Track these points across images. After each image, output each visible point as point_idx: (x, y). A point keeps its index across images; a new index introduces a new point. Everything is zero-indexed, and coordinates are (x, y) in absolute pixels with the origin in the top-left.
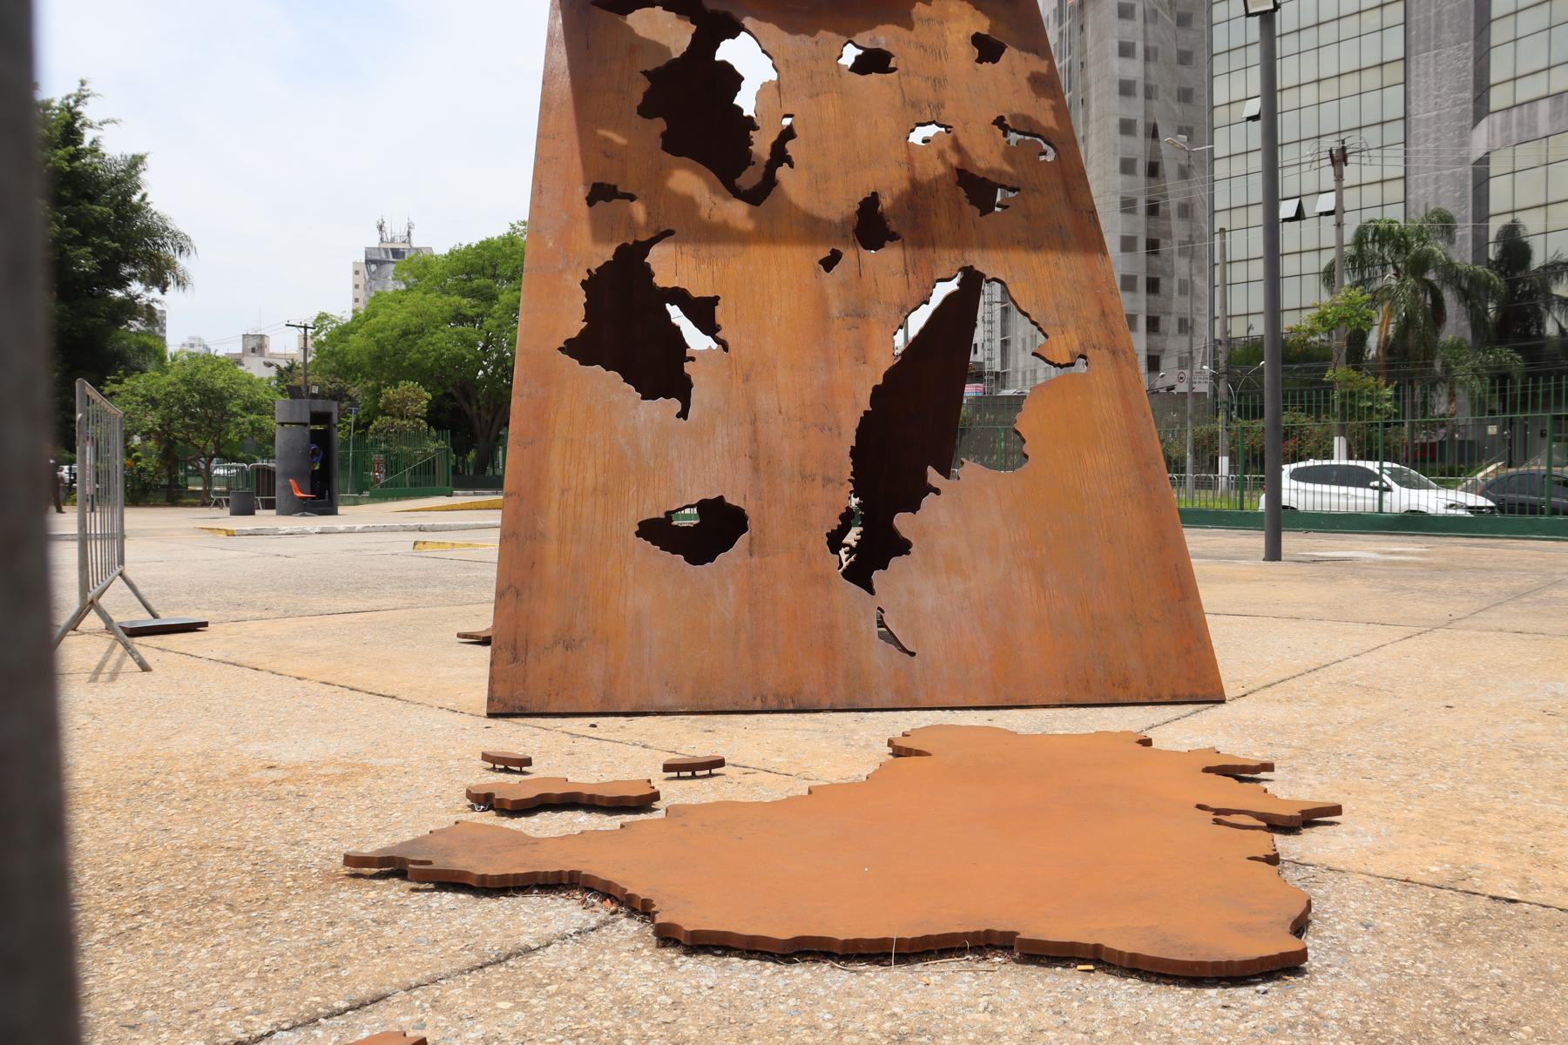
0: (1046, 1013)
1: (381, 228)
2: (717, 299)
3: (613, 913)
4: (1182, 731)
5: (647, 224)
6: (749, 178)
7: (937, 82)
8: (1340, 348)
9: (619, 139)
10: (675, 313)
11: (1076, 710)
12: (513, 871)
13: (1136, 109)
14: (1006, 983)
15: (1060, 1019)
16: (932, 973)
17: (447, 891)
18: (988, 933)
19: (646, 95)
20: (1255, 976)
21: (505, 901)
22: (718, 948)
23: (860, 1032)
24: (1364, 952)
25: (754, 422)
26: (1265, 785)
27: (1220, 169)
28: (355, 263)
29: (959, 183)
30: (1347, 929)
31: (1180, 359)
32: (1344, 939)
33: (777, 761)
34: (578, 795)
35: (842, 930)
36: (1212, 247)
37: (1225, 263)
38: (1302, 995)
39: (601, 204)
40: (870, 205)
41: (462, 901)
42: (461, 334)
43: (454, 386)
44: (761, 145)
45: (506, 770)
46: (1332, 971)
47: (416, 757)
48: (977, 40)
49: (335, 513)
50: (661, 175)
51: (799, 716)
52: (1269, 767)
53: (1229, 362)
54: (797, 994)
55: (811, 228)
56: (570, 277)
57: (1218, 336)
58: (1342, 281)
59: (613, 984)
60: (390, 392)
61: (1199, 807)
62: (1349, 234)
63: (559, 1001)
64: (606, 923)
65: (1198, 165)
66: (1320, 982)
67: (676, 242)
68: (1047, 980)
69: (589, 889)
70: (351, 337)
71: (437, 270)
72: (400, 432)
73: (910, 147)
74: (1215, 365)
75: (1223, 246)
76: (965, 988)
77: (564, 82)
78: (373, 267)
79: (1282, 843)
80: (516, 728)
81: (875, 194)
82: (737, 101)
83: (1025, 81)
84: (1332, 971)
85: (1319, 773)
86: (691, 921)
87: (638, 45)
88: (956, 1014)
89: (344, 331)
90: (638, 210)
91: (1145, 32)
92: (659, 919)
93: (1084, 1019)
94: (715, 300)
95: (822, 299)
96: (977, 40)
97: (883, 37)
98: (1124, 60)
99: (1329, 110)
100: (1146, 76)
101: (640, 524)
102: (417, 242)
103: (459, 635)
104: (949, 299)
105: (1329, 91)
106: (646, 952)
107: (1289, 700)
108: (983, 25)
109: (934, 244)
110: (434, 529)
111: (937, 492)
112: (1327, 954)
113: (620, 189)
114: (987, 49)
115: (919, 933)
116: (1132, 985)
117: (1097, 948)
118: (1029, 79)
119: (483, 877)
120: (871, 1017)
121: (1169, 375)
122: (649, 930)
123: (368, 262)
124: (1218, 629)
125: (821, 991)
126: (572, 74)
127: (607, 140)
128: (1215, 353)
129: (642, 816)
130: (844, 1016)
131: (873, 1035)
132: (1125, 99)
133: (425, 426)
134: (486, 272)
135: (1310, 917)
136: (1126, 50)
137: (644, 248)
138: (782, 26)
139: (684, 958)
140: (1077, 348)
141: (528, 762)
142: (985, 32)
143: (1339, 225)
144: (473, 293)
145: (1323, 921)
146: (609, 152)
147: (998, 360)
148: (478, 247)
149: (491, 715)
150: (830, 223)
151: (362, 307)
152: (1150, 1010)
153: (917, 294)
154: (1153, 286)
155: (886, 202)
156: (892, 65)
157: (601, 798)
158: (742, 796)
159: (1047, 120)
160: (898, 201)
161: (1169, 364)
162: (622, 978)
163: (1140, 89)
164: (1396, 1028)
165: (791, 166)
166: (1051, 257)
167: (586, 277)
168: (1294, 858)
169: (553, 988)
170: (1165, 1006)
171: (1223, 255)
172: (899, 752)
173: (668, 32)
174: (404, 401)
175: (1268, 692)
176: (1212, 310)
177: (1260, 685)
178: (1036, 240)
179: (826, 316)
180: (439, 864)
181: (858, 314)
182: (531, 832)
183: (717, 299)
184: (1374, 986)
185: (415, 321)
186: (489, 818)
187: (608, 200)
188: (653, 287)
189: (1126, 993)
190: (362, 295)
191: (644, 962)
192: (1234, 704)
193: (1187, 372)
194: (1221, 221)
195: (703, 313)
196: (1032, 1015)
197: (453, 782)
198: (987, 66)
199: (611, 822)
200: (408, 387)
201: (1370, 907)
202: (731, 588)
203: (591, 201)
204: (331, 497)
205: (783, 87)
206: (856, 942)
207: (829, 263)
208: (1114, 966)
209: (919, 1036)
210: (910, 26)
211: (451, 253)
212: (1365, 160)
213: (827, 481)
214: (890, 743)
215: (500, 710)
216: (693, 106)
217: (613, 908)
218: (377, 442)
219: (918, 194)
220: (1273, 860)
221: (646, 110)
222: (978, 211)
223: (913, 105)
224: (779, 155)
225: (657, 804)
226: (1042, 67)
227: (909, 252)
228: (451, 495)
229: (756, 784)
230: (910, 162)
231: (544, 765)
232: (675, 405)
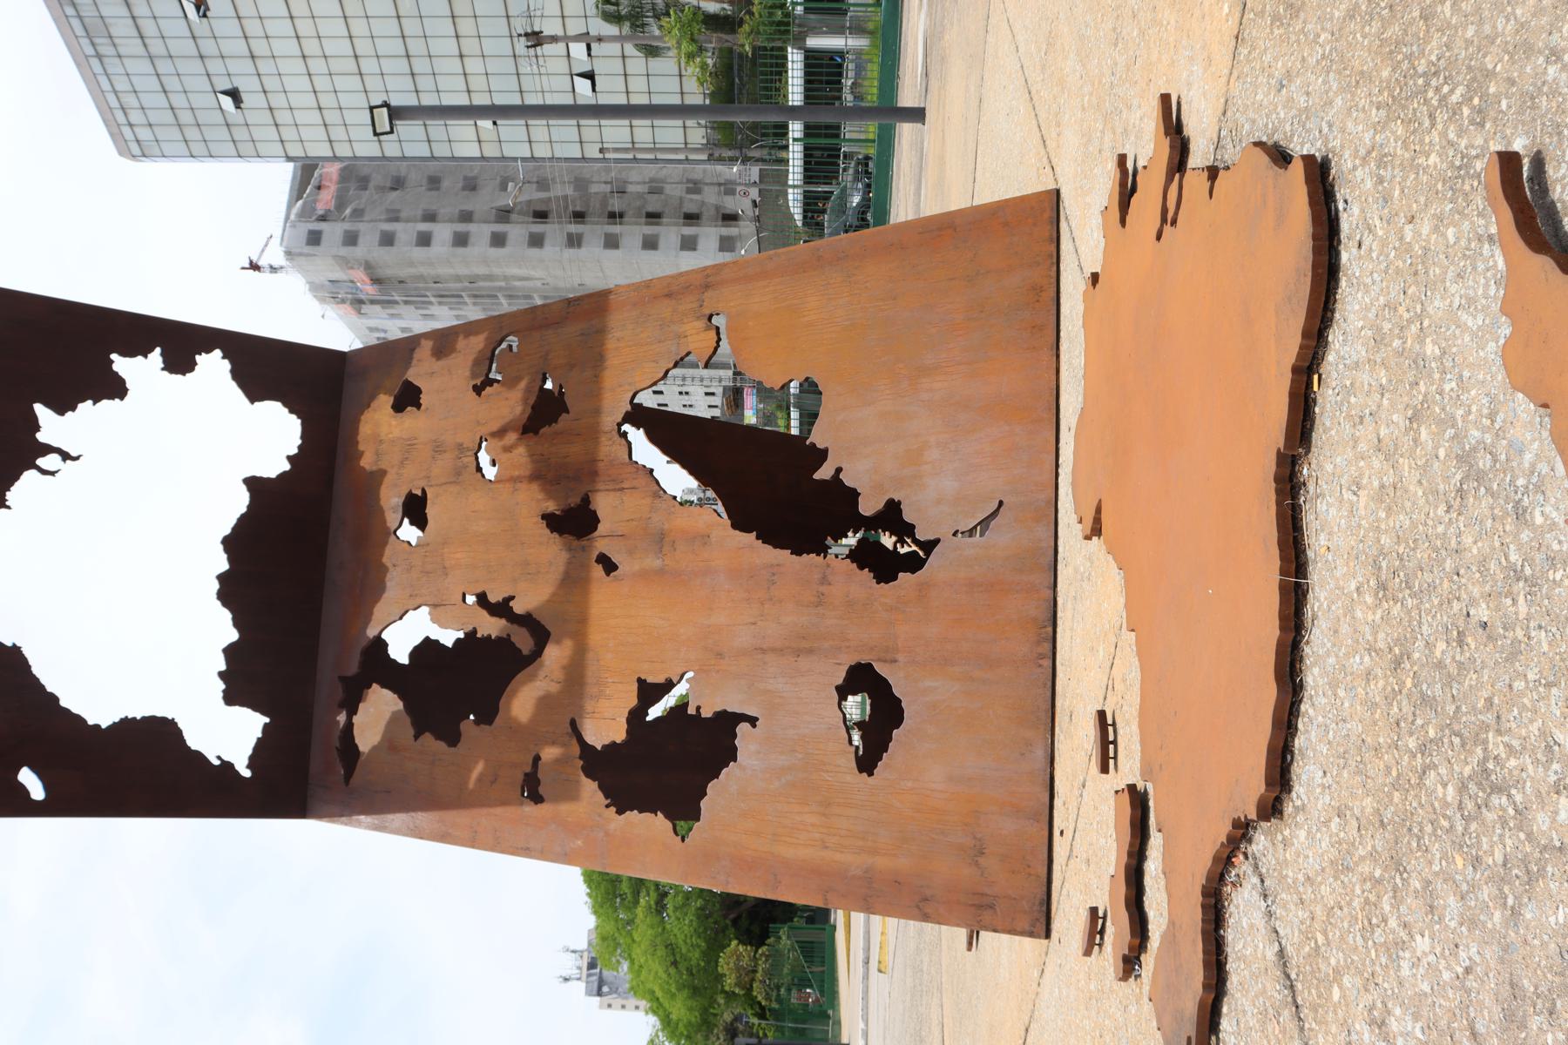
0: (1361, 431)
1: (566, 980)
3: (1246, 857)
4: (1086, 238)
5: (564, 745)
6: (523, 641)
7: (438, 448)
8: (720, 40)
9: (479, 768)
10: (655, 712)
12: (1201, 956)
13: (481, 232)
14: (1329, 468)
15: (1368, 419)
16: (1317, 543)
17: (1218, 1024)
18: (1277, 480)
19: (438, 737)
20: (1329, 210)
21: (1231, 966)
22: (1284, 758)
23: (1375, 630)
24: (1308, 94)
25: (763, 651)
26: (1140, 164)
27: (542, 151)
28: (601, 1007)
29: (536, 432)
30: (1284, 107)
32: (1294, 112)
34: (1128, 868)
35: (1270, 631)
37: (634, 149)
38: (1350, 165)
39: (541, 790)
40: (554, 523)
41: (1230, 1010)
42: (676, 909)
43: (725, 917)
44: (491, 627)
45: (1102, 932)
46: (1325, 130)
47: (1086, 1022)
48: (398, 407)
50: (515, 729)
52: (1122, 159)
53: (730, 146)
54: (1334, 685)
55: (573, 582)
56: (612, 826)
57: (705, 157)
59: (1317, 874)
60: (729, 982)
61: (1159, 238)
62: (611, 30)
63: (1334, 935)
64: (1256, 867)
66: (1336, 143)
67: (581, 717)
68: (1328, 424)
69: (1222, 877)
70: (674, 1017)
71: (610, 928)
73: (499, 480)
74: (733, 160)
75: (616, 150)
76: (1333, 511)
77: (421, 818)
78: (605, 989)
80: (1060, 912)
81: (544, 517)
82: (450, 645)
83: (440, 363)
84: (1325, 130)
85: (1130, 107)
86: (1255, 786)
87: (389, 743)
88: (1359, 526)
89: (667, 1023)
90: (549, 753)
91: (408, 221)
92: (1253, 816)
93: (1368, 393)
94: (641, 682)
95: (644, 575)
96: (398, 407)
97: (391, 500)
98: (434, 242)
99: (489, 46)
100: (451, 221)
101: (861, 771)
102: (582, 944)
104: (653, 438)
105: (470, 46)
106: (1287, 833)
108: (385, 401)
109: (595, 461)
110: (867, 949)
111: (839, 470)
113: (528, 769)
114: (408, 398)
115: (1276, 552)
116: (1335, 336)
118: (439, 358)
119: (1205, 986)
120: (1359, 614)
122: (1265, 825)
123: (599, 993)
124: (988, 194)
125: (1332, 660)
126: (414, 809)
127: (480, 780)
128: (721, 160)
129: (1151, 803)
131: (1378, 616)
133: (765, 948)
134: (610, 892)
135: (1270, 143)
137: (586, 749)
139: (1294, 794)
140: (701, 324)
141: (1094, 911)
142: (392, 399)
143: (600, 39)
144: (636, 894)
145: (1275, 130)
146: (490, 779)
147: (722, 373)
148: (589, 887)
149: (1048, 935)
150: (569, 563)
151: (643, 1004)
152: (1361, 323)
153: (642, 480)
154: (653, 217)
155: (551, 507)
156: (419, 493)
157: (1131, 845)
158: (1134, 697)
159: (478, 342)
160: (550, 495)
162: (1312, 864)
163: (461, 227)
164: (1385, 74)
165: (512, 598)
166: (611, 344)
168: (1212, 148)
169: (1320, 938)
170: (1357, 307)
171: (626, 150)
172: (1096, 530)
173: (378, 713)
174: (738, 968)
175: (1051, 144)
176: (679, 161)
178: (592, 358)
179: (661, 572)
181: (661, 541)
182: (1164, 922)
184: (1342, 90)
186: (1148, 960)
189: (1343, 346)
190: (632, 1002)
192: (1061, 180)
194: (593, 152)
195: (650, 692)
196: (1362, 447)
197: (1112, 991)
198: (424, 399)
199: (1156, 841)
200: (725, 964)
201: (1262, 79)
202: (928, 683)
203: (537, 798)
206: (1283, 618)
207: (609, 566)
208: (1316, 353)
209: (1380, 568)
211: (595, 913)
212: (538, 13)
213: (824, 580)
214: (1088, 538)
215: (1042, 925)
216: (452, 689)
217: (1241, 857)
218: (779, 1000)
219: (545, 474)
220: (1213, 172)
221: (453, 739)
223: (459, 474)
224: (501, 609)
225: (1140, 786)
226: (427, 345)
227: (601, 486)
228: (834, 927)
229: (1124, 680)
230: (513, 480)
231: (1098, 892)
232: (743, 728)
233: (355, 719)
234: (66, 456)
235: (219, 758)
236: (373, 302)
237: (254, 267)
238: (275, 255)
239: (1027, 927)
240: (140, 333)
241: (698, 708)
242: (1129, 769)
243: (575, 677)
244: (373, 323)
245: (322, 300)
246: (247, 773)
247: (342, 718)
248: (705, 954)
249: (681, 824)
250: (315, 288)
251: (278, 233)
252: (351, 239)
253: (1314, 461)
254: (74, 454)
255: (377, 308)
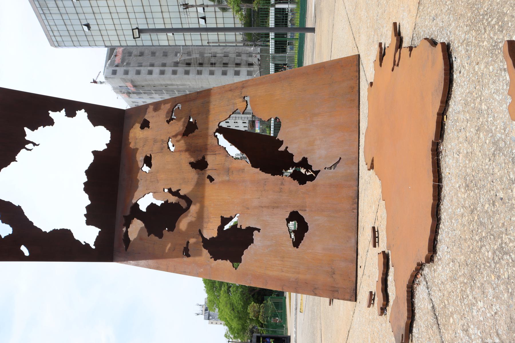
0: (460, 134)
1: (198, 314)
2: (221, 217)
3: (422, 275)
4: (368, 71)
5: (197, 238)
6: (183, 204)
7: (155, 141)
9: (169, 246)
10: (227, 227)
11: (361, 104)
12: (406, 307)
14: (449, 146)
15: (462, 130)
16: (445, 171)
17: (412, 330)
18: (432, 150)
19: (156, 235)
20: (450, 61)
21: (416, 311)
22: (434, 243)
23: (465, 200)
24: (443, 22)
25: (262, 207)
26: (386, 46)
29: (187, 136)
30: (435, 26)
31: (249, 56)
32: (438, 28)
33: (374, 208)
34: (382, 278)
35: (429, 201)
36: (213, 46)
38: (457, 46)
39: (190, 253)
40: (193, 165)
43: (250, 294)
44: (173, 199)
45: (374, 300)
46: (449, 34)
48: (142, 128)
49: (290, 337)
50: (181, 233)
51: (360, 197)
52: (380, 44)
53: (251, 41)
54: (451, 219)
55: (200, 185)
56: (213, 264)
58: (225, 5)
59: (445, 281)
60: (251, 315)
61: (393, 70)
63: (451, 301)
64: (425, 278)
65: (188, 50)
66: (452, 38)
67: (203, 229)
68: (449, 132)
69: (413, 282)
70: (233, 327)
71: (212, 298)
72: (265, 313)
73: (175, 151)
74: (251, 45)
75: (213, 42)
76: (451, 161)
77: (151, 262)
78: (211, 318)
79: (405, 44)
81: (190, 163)
82: (159, 205)
84: (449, 34)
85: (383, 27)
86: (425, 252)
87: (140, 237)
88: (460, 166)
89: (231, 329)
90: (192, 241)
91: (145, 66)
92: (424, 262)
96: (142, 128)
97: (140, 158)
98: (153, 73)
100: (159, 66)
103: (330, 305)
104: (226, 137)
107: (359, 33)
108: (138, 126)
109: (206, 145)
110: (296, 305)
111: (287, 148)
112: (443, 34)
113: (185, 246)
114: (145, 125)
116: (451, 103)
117: (438, 114)
118: (155, 112)
119: (408, 318)
120: (459, 195)
121: (254, 60)
123: (209, 319)
124: (336, 56)
125: (450, 210)
126: (148, 259)
127: (169, 249)
129: (390, 257)
130: (459, 204)
131: (466, 196)
132: (166, 73)
133: (263, 304)
134: (213, 286)
135: (430, 38)
136: (150, 73)
137: (204, 239)
138: (136, 190)
139: (437, 255)
140: (241, 100)
141: (371, 292)
143: (207, 6)
144: (221, 287)
145: (432, 34)
146: (173, 249)
147: (248, 116)
148: (205, 284)
149: (356, 301)
150: (198, 179)
151: (223, 322)
153: (222, 151)
154: (225, 64)
155: (192, 160)
157: (383, 271)
158: (384, 223)
159: (168, 106)
160: (192, 156)
161: (251, 60)
162: (444, 278)
163: (162, 68)
164: (469, 15)
165: (180, 190)
166: (212, 106)
167: (213, 259)
168: (410, 40)
169: (446, 302)
170: (459, 93)
171: (216, 42)
172: (372, 167)
173: (136, 227)
174: (254, 311)
175: (357, 39)
176: (234, 46)
177: (354, 42)
178: (206, 111)
179: (228, 181)
180: (403, 332)
181: (228, 171)
183: (221, 217)
184: (454, 20)
185: (229, 306)
186: (389, 309)
187: (188, 250)
188: (217, 237)
190: (219, 322)
191: (439, 269)
192: (360, 51)
193: (253, 55)
195: (225, 221)
196: (461, 139)
198: (150, 125)
199: (391, 270)
200: (250, 309)
202: (316, 218)
203: (188, 256)
204: (285, 338)
205: (155, 191)
206: (434, 196)
207: (211, 179)
208: (445, 108)
209: (466, 180)
210: (137, 149)
213: (282, 184)
214: (369, 170)
215: (354, 297)
216: (162, 219)
217: (420, 275)
218: (267, 321)
219: (190, 149)
220: (411, 48)
221: (160, 236)
222: (196, 130)
223: (162, 149)
224: (176, 194)
226: (151, 107)
227: (208, 153)
229: (381, 217)
230: (180, 151)
231: (372, 287)
232: (255, 232)
233: (129, 230)
234: (34, 144)
235: (85, 242)
236: (134, 93)
237: (95, 82)
238: (102, 78)
239: (349, 298)
240: (58, 104)
241: (241, 226)
242: (383, 246)
243: (200, 216)
244: (134, 100)
245: (117, 93)
246: (94, 247)
247: (124, 229)
248: (243, 307)
249: (235, 264)
250: (115, 89)
251: (102, 71)
252: (126, 73)
253: (444, 144)
254: (37, 144)
255: (135, 95)
